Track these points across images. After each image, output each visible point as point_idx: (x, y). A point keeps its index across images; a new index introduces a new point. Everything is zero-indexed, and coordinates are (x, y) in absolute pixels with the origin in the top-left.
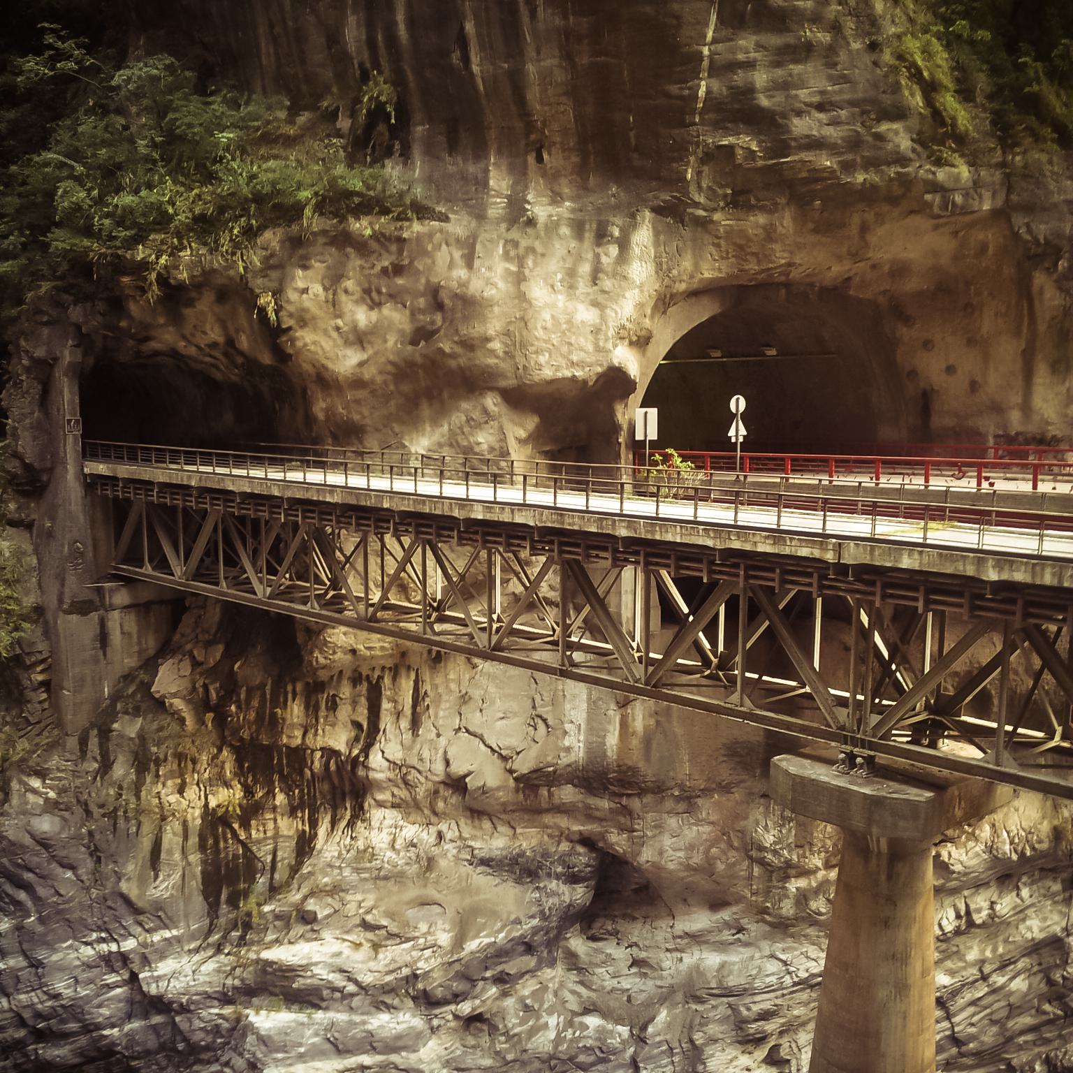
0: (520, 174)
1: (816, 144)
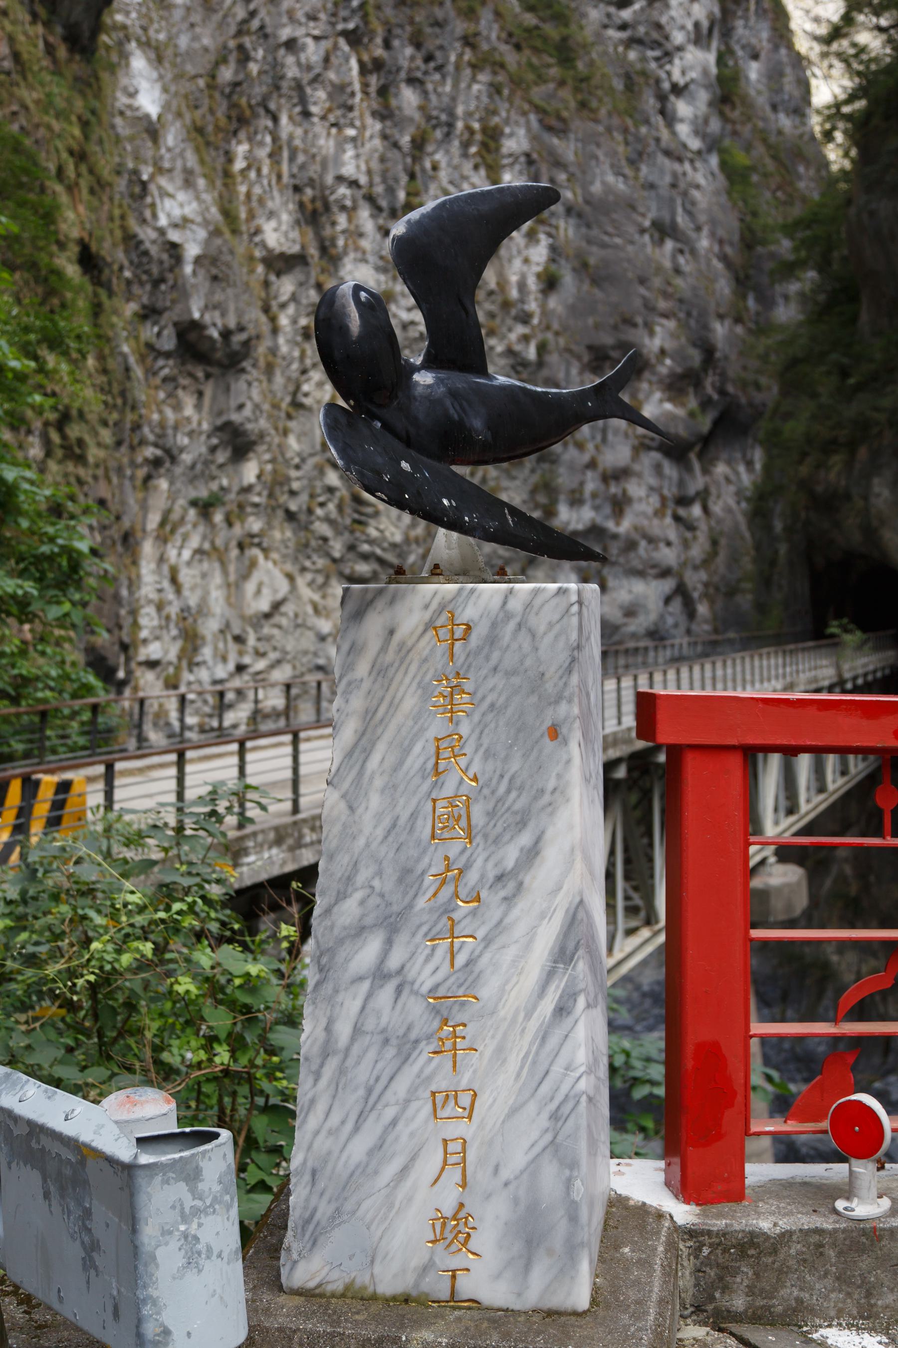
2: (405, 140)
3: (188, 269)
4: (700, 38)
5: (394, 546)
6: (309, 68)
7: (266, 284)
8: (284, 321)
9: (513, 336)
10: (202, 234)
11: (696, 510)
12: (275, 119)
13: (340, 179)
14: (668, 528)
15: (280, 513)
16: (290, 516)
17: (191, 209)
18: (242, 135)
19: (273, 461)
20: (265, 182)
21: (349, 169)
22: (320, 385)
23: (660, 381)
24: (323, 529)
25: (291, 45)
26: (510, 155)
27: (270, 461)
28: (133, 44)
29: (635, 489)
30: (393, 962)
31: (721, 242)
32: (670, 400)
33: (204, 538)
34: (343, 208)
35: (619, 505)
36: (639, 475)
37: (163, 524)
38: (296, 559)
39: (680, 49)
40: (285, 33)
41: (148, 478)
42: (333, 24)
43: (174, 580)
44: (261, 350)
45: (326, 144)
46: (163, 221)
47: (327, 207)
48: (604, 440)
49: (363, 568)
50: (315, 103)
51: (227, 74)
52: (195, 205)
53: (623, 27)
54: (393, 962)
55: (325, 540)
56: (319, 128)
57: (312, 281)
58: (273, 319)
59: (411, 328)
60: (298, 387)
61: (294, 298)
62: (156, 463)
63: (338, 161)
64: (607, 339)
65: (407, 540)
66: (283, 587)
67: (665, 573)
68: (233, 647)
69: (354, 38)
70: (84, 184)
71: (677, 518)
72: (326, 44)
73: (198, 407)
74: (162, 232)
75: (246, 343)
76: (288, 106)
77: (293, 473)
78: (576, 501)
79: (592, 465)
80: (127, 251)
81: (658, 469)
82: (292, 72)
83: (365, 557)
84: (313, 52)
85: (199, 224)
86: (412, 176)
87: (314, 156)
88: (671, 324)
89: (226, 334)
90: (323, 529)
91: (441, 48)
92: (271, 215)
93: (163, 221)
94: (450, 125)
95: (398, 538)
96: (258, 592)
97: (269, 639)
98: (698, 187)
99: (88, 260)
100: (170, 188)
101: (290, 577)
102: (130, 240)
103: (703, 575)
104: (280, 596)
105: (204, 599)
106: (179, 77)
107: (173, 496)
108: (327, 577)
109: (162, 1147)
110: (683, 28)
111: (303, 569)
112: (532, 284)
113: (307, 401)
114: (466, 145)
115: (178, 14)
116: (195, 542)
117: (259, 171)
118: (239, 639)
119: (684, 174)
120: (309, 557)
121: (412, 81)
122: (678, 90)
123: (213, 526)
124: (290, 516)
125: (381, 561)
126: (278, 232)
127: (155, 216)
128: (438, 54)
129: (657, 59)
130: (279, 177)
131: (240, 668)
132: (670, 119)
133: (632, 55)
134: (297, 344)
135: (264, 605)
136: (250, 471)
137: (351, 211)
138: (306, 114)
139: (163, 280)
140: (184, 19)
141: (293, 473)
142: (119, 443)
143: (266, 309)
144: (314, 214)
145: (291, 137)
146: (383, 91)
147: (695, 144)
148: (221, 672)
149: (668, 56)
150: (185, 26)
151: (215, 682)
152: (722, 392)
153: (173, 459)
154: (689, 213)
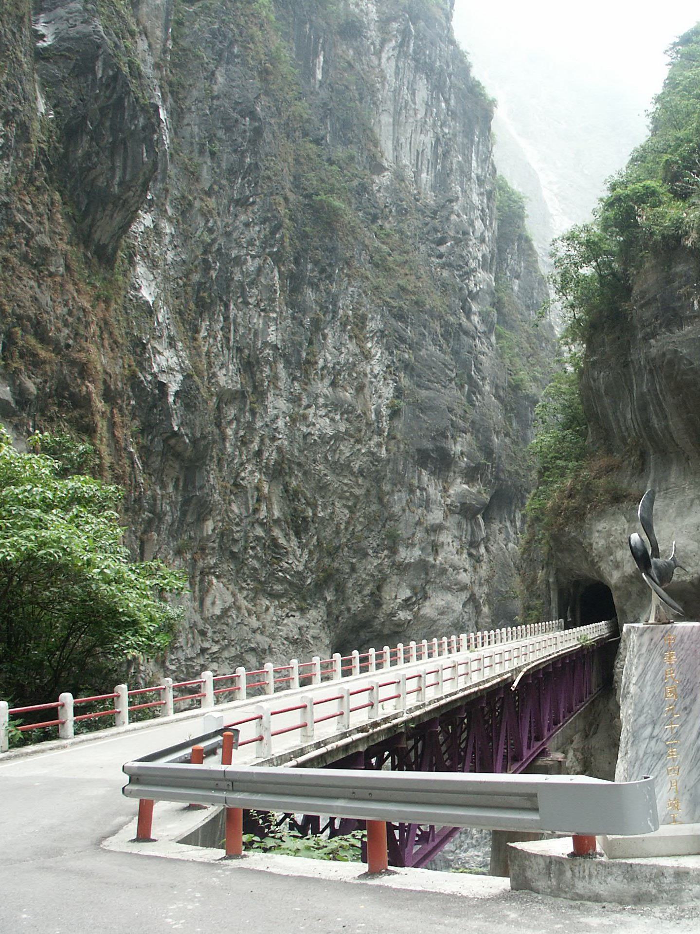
2: (307, 321)
3: (171, 399)
4: (485, 265)
5: (298, 572)
6: (248, 275)
8: (229, 432)
9: (372, 443)
10: (179, 377)
11: (482, 550)
12: (227, 306)
13: (265, 344)
14: (463, 560)
15: (227, 553)
16: (233, 556)
17: (173, 361)
18: (206, 315)
19: (222, 521)
20: (219, 345)
21: (272, 338)
22: (252, 472)
23: (461, 472)
26: (372, 331)
27: (220, 521)
28: (139, 257)
29: (445, 538)
30: (655, 734)
31: (497, 387)
32: (467, 483)
34: (268, 362)
35: (436, 548)
36: (447, 529)
38: (236, 583)
39: (474, 270)
40: (234, 253)
42: (264, 249)
45: (258, 322)
46: (155, 369)
47: (258, 363)
49: (278, 587)
50: (251, 297)
51: (196, 277)
52: (175, 359)
53: (440, 256)
54: (655, 734)
55: (255, 569)
56: (254, 313)
57: (248, 408)
59: (309, 438)
60: (238, 474)
61: (236, 418)
62: (150, 522)
64: (428, 445)
66: (230, 600)
67: (463, 588)
68: (199, 638)
69: (278, 259)
71: (470, 555)
73: (176, 487)
74: (155, 376)
75: (206, 447)
76: (235, 298)
77: (235, 529)
78: (410, 546)
79: (419, 523)
81: (459, 525)
82: (238, 277)
84: (251, 265)
85: (177, 371)
86: (311, 343)
87: (250, 329)
88: (468, 436)
91: (330, 265)
92: (223, 366)
93: (155, 369)
94: (335, 313)
96: (213, 603)
97: (221, 631)
98: (484, 354)
99: (109, 396)
100: (159, 348)
101: (234, 595)
102: (133, 380)
103: (486, 589)
104: (227, 605)
106: (166, 279)
108: (256, 593)
109: (403, 805)
110: (476, 258)
111: (242, 589)
112: (385, 411)
114: (344, 325)
115: (167, 239)
117: (215, 338)
118: (203, 633)
119: (475, 346)
120: (245, 581)
121: (312, 284)
122: (473, 296)
124: (233, 556)
126: (227, 377)
127: (151, 367)
128: (329, 270)
129: (460, 276)
130: (228, 340)
131: (203, 651)
132: (468, 313)
133: (445, 274)
134: (237, 447)
135: (218, 612)
137: (272, 365)
139: (155, 406)
140: (171, 242)
141: (235, 529)
143: (218, 425)
144: (249, 366)
147: (481, 328)
148: (190, 653)
149: (467, 274)
151: (187, 659)
152: (497, 478)
153: (161, 520)
154: (479, 370)
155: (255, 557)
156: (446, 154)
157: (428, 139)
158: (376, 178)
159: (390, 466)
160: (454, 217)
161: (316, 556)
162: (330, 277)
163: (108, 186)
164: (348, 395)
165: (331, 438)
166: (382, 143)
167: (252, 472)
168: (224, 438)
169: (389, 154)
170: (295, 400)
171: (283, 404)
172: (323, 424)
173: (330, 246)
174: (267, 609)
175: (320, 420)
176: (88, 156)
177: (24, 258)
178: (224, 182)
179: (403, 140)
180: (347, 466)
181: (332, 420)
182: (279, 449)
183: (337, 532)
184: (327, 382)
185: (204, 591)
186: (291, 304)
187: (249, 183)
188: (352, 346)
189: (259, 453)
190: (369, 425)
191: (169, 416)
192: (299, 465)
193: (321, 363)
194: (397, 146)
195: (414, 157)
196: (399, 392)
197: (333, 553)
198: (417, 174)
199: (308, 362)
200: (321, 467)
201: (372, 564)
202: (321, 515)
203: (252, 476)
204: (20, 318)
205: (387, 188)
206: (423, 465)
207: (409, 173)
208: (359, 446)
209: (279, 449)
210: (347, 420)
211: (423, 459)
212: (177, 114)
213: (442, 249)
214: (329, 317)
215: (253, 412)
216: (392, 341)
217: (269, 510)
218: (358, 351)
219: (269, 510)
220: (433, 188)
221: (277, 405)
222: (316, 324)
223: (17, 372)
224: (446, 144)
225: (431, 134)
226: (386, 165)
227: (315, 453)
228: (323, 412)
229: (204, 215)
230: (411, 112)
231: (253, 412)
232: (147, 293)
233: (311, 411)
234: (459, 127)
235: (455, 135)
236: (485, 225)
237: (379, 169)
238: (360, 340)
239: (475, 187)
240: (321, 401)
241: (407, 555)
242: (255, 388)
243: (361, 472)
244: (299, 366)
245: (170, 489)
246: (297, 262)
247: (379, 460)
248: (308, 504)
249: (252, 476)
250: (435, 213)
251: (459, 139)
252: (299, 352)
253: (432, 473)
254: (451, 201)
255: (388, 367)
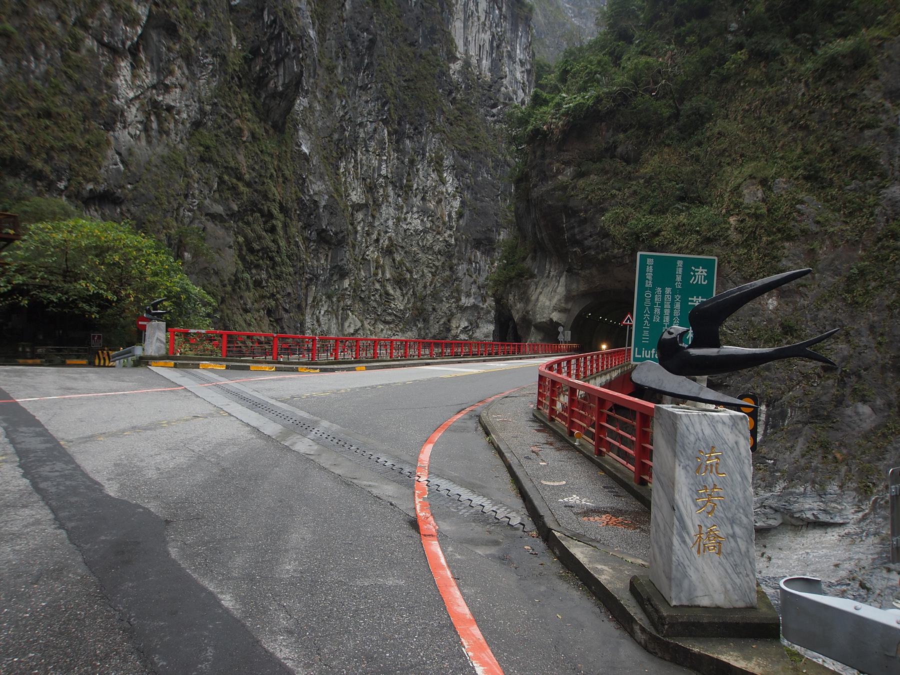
0: (550, 263)
1: (590, 248)
6: (368, 134)
7: (352, 214)
8: (359, 228)
9: (446, 235)
10: (326, 197)
12: (356, 153)
16: (362, 299)
21: (384, 172)
22: (373, 252)
24: (375, 304)
25: (361, 125)
33: (329, 306)
37: (313, 301)
41: (307, 286)
43: (318, 321)
44: (350, 240)
47: (376, 187)
48: (479, 274)
49: (389, 318)
53: (493, 116)
56: (372, 156)
58: (355, 228)
62: (311, 280)
63: (379, 169)
65: (405, 309)
66: (359, 324)
69: (385, 122)
70: (281, 180)
72: (374, 125)
73: (326, 260)
77: (362, 284)
78: (468, 295)
79: (475, 282)
80: (298, 204)
82: (362, 135)
83: (390, 314)
86: (409, 175)
89: (336, 234)
90: (375, 304)
91: (420, 125)
93: (312, 193)
94: (424, 155)
95: (402, 308)
99: (283, 209)
101: (362, 321)
102: (300, 201)
105: (329, 328)
107: (317, 292)
108: (376, 321)
113: (368, 258)
114: (429, 163)
116: (325, 308)
121: (409, 137)
123: (332, 302)
124: (362, 299)
125: (395, 315)
126: (356, 196)
127: (308, 191)
136: (346, 283)
138: (367, 151)
141: (362, 284)
142: (295, 273)
143: (352, 224)
144: (371, 189)
145: (361, 160)
146: (397, 142)
150: (320, 118)
153: (317, 279)
155: (375, 300)
156: (498, 47)
157: (487, 36)
158: (451, 65)
159: (457, 248)
160: (503, 89)
161: (412, 301)
162: (420, 133)
163: (276, 87)
164: (432, 205)
165: (421, 231)
166: (456, 41)
167: (373, 252)
168: (356, 232)
169: (461, 48)
170: (399, 208)
171: (391, 211)
172: (415, 222)
173: (420, 112)
174: (382, 330)
175: (414, 221)
176: (262, 69)
177: (228, 133)
178: (351, 75)
179: (470, 38)
180: (431, 248)
181: (422, 220)
182: (390, 238)
183: (425, 287)
184: (419, 197)
185: (345, 319)
186: (397, 150)
187: (368, 75)
188: (434, 176)
189: (377, 241)
190: (444, 223)
191: (320, 220)
192: (402, 247)
193: (415, 186)
194: (466, 43)
195: (477, 50)
196: (463, 203)
197: (423, 299)
198: (479, 61)
199: (406, 186)
200: (415, 249)
201: (445, 306)
202: (415, 277)
203: (372, 254)
204: (226, 168)
205: (459, 72)
206: (478, 248)
207: (474, 61)
208: (438, 236)
209: (390, 238)
210: (431, 221)
211: (477, 244)
212: (322, 33)
213: (495, 111)
214: (419, 158)
215: (373, 217)
216: (459, 171)
217: (383, 273)
218: (438, 179)
219: (383, 274)
220: (490, 70)
221: (387, 212)
222: (412, 162)
223: (227, 199)
224: (499, 39)
225: (489, 33)
226: (459, 56)
227: (412, 240)
228: (416, 216)
229: (339, 97)
230: (476, 19)
231: (373, 217)
232: (305, 149)
233: (409, 215)
234: (508, 26)
235: (505, 32)
236: (525, 93)
237: (454, 59)
238: (440, 173)
239: (518, 67)
240: (415, 209)
241: (465, 301)
242: (374, 202)
243: (440, 252)
244: (401, 188)
245: (322, 262)
246: (399, 124)
247: (450, 245)
248: (407, 270)
249: (372, 254)
250: (490, 87)
251: (508, 35)
252: (401, 180)
253: (483, 253)
254: (502, 78)
255: (457, 188)
